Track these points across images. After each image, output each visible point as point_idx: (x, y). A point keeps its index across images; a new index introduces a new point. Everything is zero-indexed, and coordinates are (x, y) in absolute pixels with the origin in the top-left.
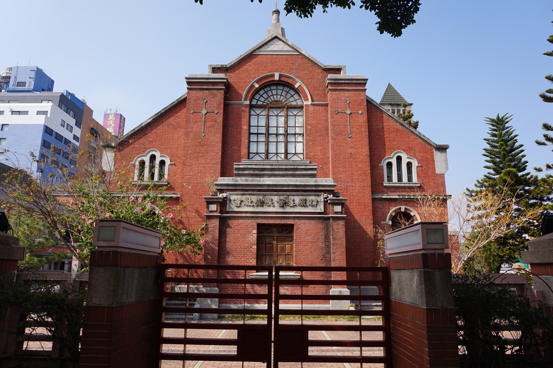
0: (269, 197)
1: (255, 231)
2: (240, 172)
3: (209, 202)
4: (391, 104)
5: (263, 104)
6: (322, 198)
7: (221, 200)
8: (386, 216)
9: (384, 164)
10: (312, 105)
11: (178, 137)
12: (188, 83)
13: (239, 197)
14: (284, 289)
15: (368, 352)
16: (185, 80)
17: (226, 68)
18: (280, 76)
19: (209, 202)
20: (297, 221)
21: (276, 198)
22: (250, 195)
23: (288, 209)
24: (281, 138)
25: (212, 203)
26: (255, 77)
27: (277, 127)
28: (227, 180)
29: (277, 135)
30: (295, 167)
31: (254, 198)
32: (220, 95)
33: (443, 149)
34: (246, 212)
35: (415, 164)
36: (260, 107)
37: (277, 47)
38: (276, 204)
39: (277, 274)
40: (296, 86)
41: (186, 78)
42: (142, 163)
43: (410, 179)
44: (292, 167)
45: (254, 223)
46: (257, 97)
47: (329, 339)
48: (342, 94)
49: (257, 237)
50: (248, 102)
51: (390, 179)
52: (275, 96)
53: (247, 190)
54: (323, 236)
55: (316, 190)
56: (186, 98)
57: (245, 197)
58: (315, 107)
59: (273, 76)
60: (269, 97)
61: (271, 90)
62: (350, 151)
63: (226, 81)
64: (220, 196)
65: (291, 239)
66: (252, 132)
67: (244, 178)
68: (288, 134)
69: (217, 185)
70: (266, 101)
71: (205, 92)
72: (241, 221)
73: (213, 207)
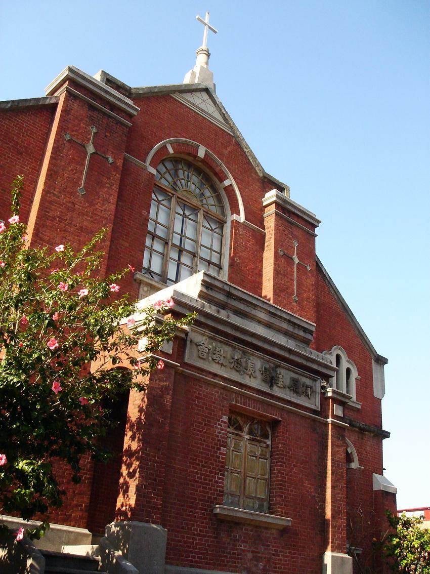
34: (215, 375)
37: (199, 102)
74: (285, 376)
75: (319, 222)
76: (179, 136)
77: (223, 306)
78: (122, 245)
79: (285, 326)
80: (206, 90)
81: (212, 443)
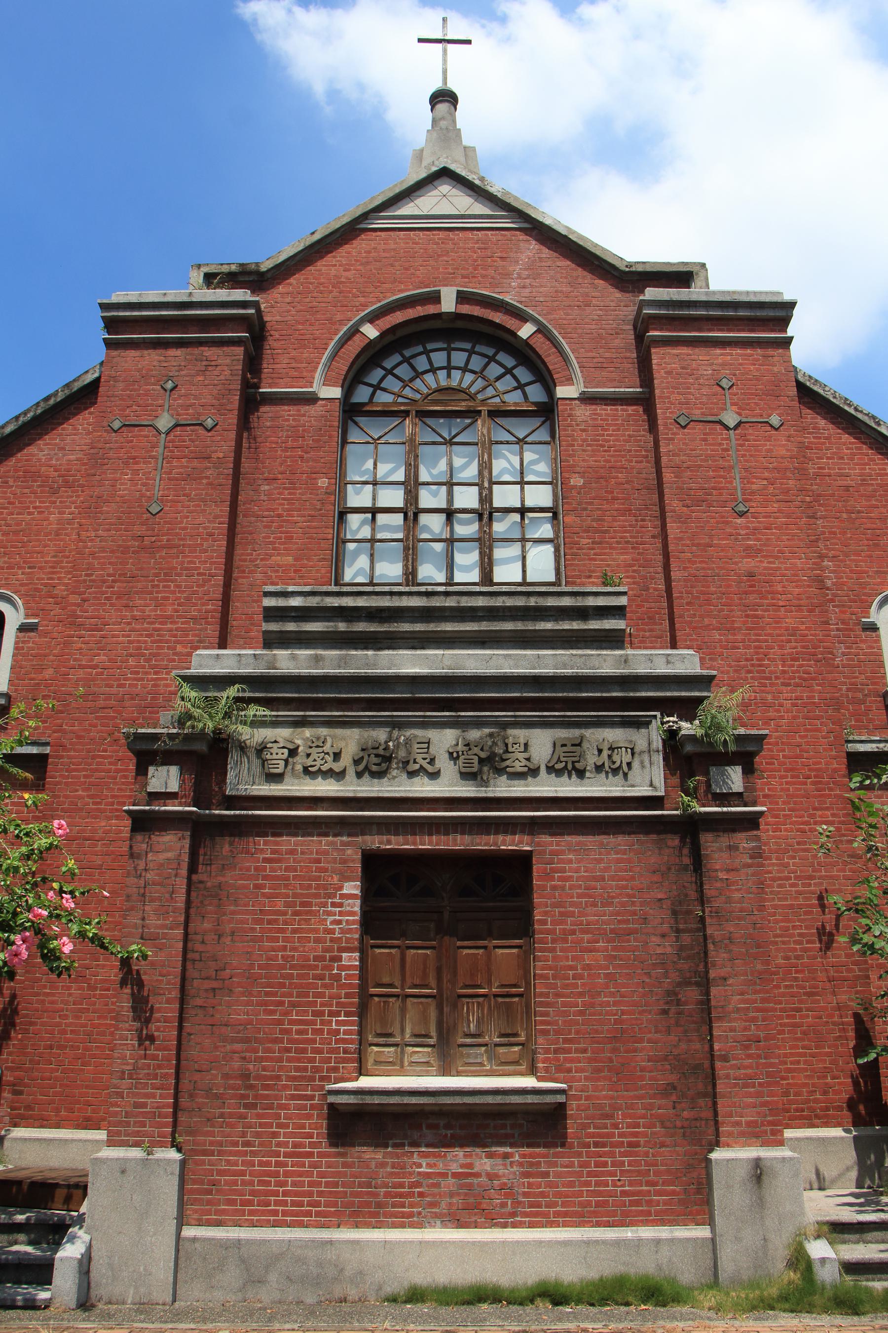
0: (419, 733)
1: (352, 888)
2: (291, 627)
3: (147, 753)
5: (395, 403)
6: (655, 735)
7: (201, 747)
11: (60, 522)
12: (111, 325)
13: (283, 733)
14: (490, 1156)
16: (100, 313)
17: (262, 274)
18: (463, 298)
19: (147, 753)
21: (444, 739)
22: (330, 723)
23: (503, 788)
24: (466, 529)
25: (168, 758)
26: (365, 305)
28: (233, 662)
29: (450, 514)
30: (532, 602)
31: (349, 741)
32: (228, 362)
38: (444, 763)
41: (104, 307)
44: (520, 602)
45: (349, 850)
48: (700, 355)
49: (365, 914)
52: (442, 374)
53: (318, 704)
54: (667, 904)
55: (628, 701)
56: (96, 383)
57: (308, 732)
58: (599, 409)
59: (435, 298)
61: (427, 352)
62: (747, 564)
63: (253, 311)
65: (519, 923)
67: (304, 653)
68: (493, 511)
70: (407, 392)
71: (172, 352)
72: (288, 842)
73: (166, 778)
75: (792, 305)
76: (388, 294)
78: (278, 565)
80: (445, 174)
81: (314, 949)
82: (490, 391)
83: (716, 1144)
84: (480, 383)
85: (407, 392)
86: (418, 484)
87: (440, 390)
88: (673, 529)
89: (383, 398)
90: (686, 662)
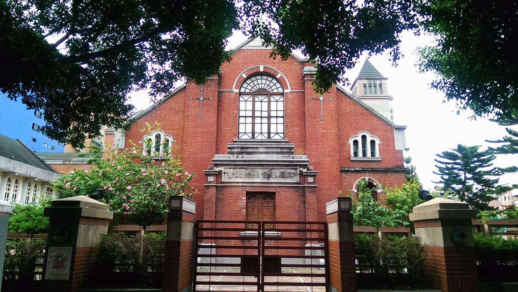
1: (244, 198)
4: (367, 79)
8: (353, 185)
9: (351, 142)
10: (290, 92)
15: (316, 280)
20: (278, 189)
23: (272, 180)
27: (261, 117)
31: (244, 171)
33: (401, 129)
35: (377, 142)
36: (248, 94)
38: (260, 176)
39: (263, 233)
40: (278, 77)
42: (356, 142)
43: (373, 154)
46: (245, 85)
47: (303, 282)
50: (238, 91)
51: (356, 154)
55: (293, 165)
60: (255, 85)
62: (322, 131)
64: (217, 169)
66: (240, 115)
69: (213, 161)
70: (253, 89)
73: (211, 179)
74: (277, 172)
77: (241, 153)
79: (275, 150)
82: (271, 89)
83: (168, 213)
84: (268, 87)
85: (253, 89)
86: (255, 111)
87: (260, 89)
88: (307, 123)
89: (247, 91)
90: (304, 158)
